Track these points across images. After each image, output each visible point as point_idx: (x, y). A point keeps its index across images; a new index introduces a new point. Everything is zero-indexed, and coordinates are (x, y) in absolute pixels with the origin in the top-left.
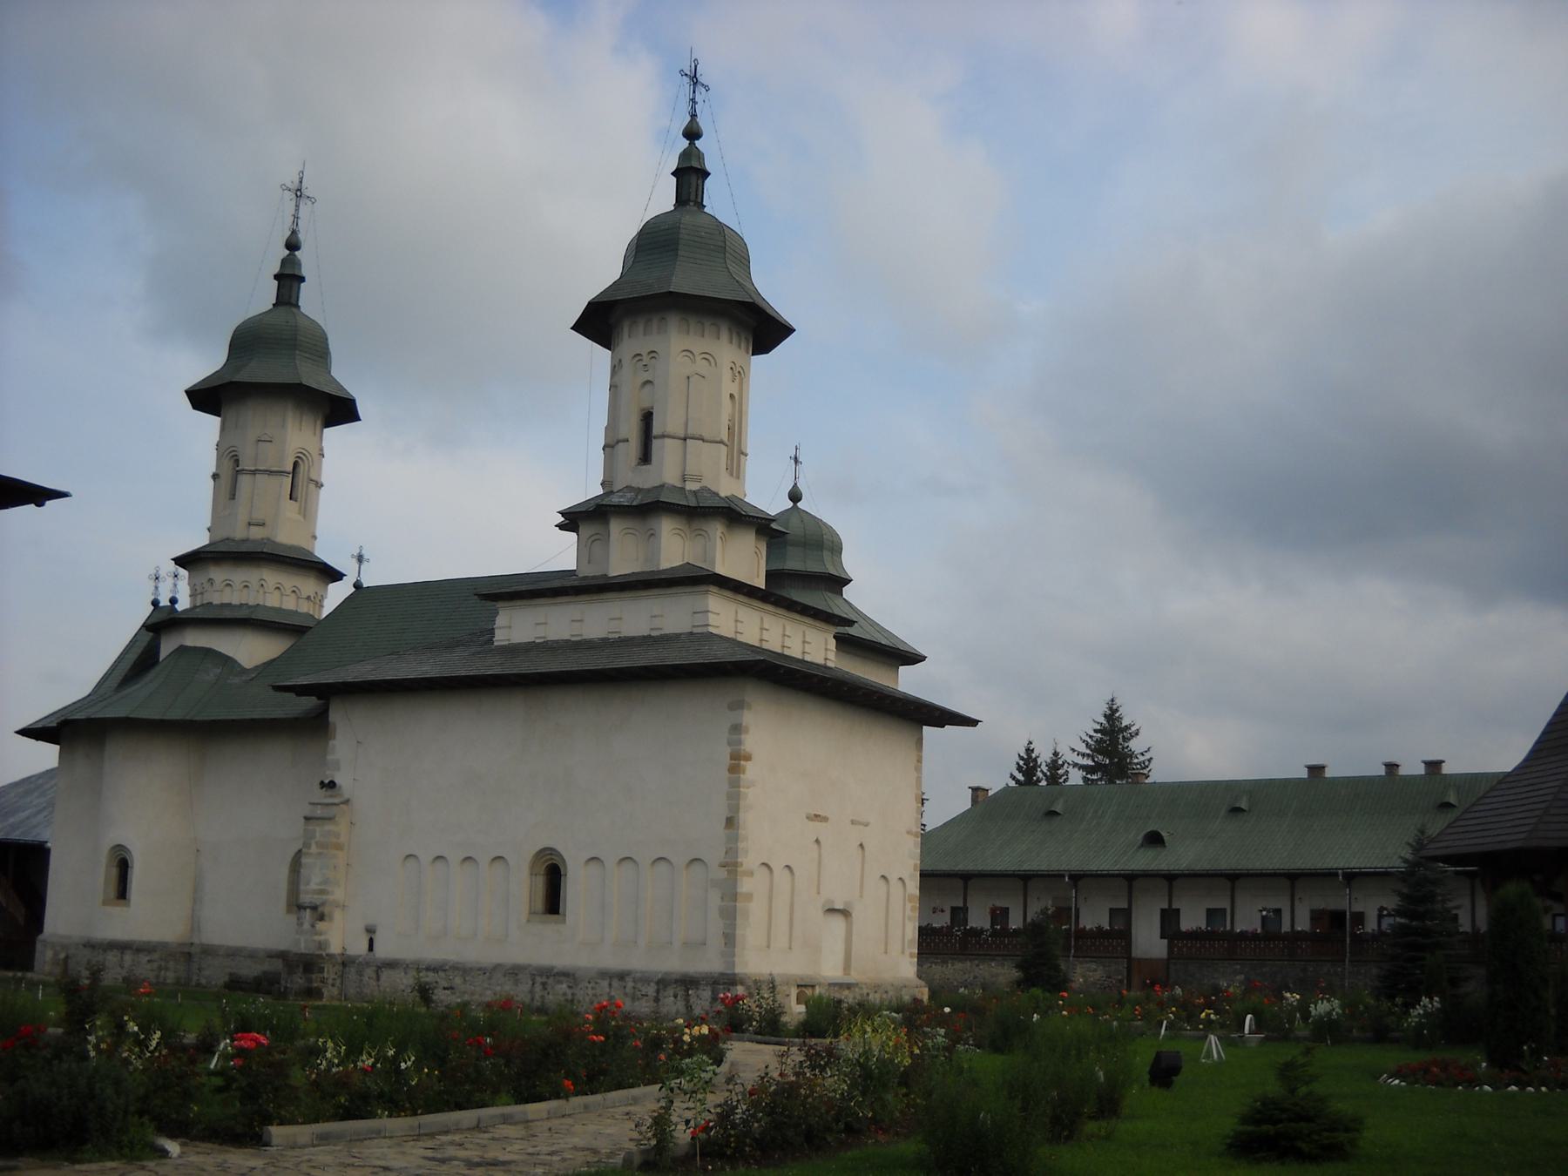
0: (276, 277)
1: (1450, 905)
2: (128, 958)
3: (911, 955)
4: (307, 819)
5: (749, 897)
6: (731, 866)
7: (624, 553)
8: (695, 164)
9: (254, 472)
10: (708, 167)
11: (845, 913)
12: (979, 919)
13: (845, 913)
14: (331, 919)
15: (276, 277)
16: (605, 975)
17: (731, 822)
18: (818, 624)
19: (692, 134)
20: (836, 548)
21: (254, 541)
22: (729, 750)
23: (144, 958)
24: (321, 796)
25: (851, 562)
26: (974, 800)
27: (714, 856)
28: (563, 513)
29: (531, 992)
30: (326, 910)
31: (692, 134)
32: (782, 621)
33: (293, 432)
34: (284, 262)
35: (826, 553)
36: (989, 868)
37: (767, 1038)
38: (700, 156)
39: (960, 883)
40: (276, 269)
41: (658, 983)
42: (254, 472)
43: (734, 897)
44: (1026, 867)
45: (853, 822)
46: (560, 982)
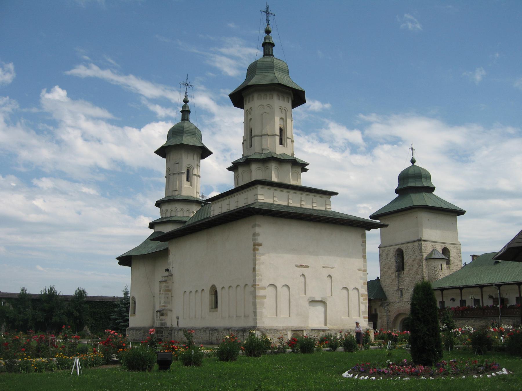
2: (135, 332)
3: (364, 318)
4: (160, 282)
5: (264, 297)
6: (254, 286)
11: (323, 302)
12: (470, 303)
13: (323, 302)
14: (167, 315)
15: (181, 112)
16: (205, 329)
17: (254, 269)
18: (239, 193)
19: (268, 32)
20: (428, 177)
22: (252, 243)
23: (138, 332)
24: (167, 273)
25: (434, 181)
26: (473, 259)
27: (250, 284)
29: (209, 337)
30: (164, 312)
31: (268, 32)
32: (300, 196)
33: (187, 160)
35: (423, 179)
36: (471, 284)
39: (479, 290)
41: (237, 331)
43: (255, 297)
44: (480, 283)
45: (323, 267)
46: (215, 333)
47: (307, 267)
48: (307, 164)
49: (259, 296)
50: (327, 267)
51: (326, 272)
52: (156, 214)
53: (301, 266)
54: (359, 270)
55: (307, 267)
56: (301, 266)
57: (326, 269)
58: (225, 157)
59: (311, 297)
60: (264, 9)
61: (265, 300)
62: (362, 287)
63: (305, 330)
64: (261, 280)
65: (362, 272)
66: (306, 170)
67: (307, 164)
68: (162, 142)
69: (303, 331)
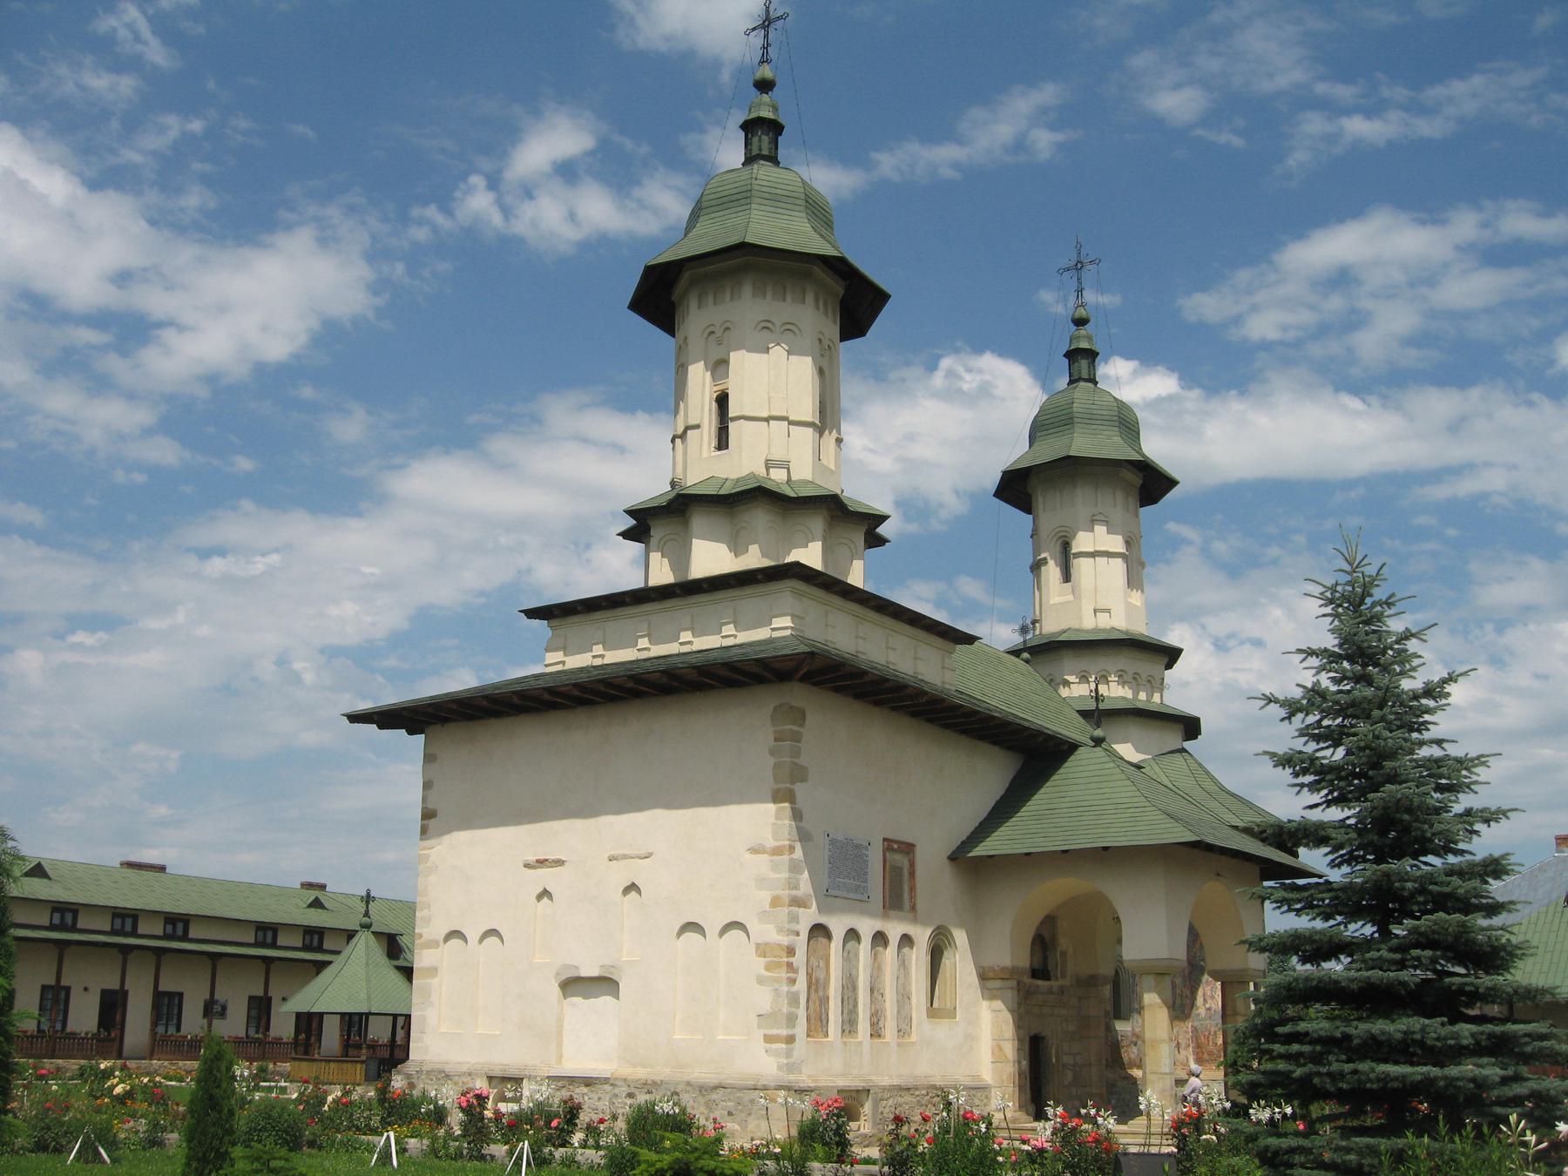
5: (433, 971)
9: (1093, 555)
21: (1104, 630)
28: (631, 513)
42: (1093, 555)
47: (560, 863)
49: (422, 969)
50: (625, 857)
51: (622, 874)
52: (771, 761)
53: (541, 863)
54: (755, 850)
55: (560, 863)
56: (541, 863)
58: (1203, 627)
61: (435, 981)
62: (763, 916)
63: (529, 1078)
64: (428, 920)
65: (765, 857)
68: (1014, 451)
69: (518, 1081)
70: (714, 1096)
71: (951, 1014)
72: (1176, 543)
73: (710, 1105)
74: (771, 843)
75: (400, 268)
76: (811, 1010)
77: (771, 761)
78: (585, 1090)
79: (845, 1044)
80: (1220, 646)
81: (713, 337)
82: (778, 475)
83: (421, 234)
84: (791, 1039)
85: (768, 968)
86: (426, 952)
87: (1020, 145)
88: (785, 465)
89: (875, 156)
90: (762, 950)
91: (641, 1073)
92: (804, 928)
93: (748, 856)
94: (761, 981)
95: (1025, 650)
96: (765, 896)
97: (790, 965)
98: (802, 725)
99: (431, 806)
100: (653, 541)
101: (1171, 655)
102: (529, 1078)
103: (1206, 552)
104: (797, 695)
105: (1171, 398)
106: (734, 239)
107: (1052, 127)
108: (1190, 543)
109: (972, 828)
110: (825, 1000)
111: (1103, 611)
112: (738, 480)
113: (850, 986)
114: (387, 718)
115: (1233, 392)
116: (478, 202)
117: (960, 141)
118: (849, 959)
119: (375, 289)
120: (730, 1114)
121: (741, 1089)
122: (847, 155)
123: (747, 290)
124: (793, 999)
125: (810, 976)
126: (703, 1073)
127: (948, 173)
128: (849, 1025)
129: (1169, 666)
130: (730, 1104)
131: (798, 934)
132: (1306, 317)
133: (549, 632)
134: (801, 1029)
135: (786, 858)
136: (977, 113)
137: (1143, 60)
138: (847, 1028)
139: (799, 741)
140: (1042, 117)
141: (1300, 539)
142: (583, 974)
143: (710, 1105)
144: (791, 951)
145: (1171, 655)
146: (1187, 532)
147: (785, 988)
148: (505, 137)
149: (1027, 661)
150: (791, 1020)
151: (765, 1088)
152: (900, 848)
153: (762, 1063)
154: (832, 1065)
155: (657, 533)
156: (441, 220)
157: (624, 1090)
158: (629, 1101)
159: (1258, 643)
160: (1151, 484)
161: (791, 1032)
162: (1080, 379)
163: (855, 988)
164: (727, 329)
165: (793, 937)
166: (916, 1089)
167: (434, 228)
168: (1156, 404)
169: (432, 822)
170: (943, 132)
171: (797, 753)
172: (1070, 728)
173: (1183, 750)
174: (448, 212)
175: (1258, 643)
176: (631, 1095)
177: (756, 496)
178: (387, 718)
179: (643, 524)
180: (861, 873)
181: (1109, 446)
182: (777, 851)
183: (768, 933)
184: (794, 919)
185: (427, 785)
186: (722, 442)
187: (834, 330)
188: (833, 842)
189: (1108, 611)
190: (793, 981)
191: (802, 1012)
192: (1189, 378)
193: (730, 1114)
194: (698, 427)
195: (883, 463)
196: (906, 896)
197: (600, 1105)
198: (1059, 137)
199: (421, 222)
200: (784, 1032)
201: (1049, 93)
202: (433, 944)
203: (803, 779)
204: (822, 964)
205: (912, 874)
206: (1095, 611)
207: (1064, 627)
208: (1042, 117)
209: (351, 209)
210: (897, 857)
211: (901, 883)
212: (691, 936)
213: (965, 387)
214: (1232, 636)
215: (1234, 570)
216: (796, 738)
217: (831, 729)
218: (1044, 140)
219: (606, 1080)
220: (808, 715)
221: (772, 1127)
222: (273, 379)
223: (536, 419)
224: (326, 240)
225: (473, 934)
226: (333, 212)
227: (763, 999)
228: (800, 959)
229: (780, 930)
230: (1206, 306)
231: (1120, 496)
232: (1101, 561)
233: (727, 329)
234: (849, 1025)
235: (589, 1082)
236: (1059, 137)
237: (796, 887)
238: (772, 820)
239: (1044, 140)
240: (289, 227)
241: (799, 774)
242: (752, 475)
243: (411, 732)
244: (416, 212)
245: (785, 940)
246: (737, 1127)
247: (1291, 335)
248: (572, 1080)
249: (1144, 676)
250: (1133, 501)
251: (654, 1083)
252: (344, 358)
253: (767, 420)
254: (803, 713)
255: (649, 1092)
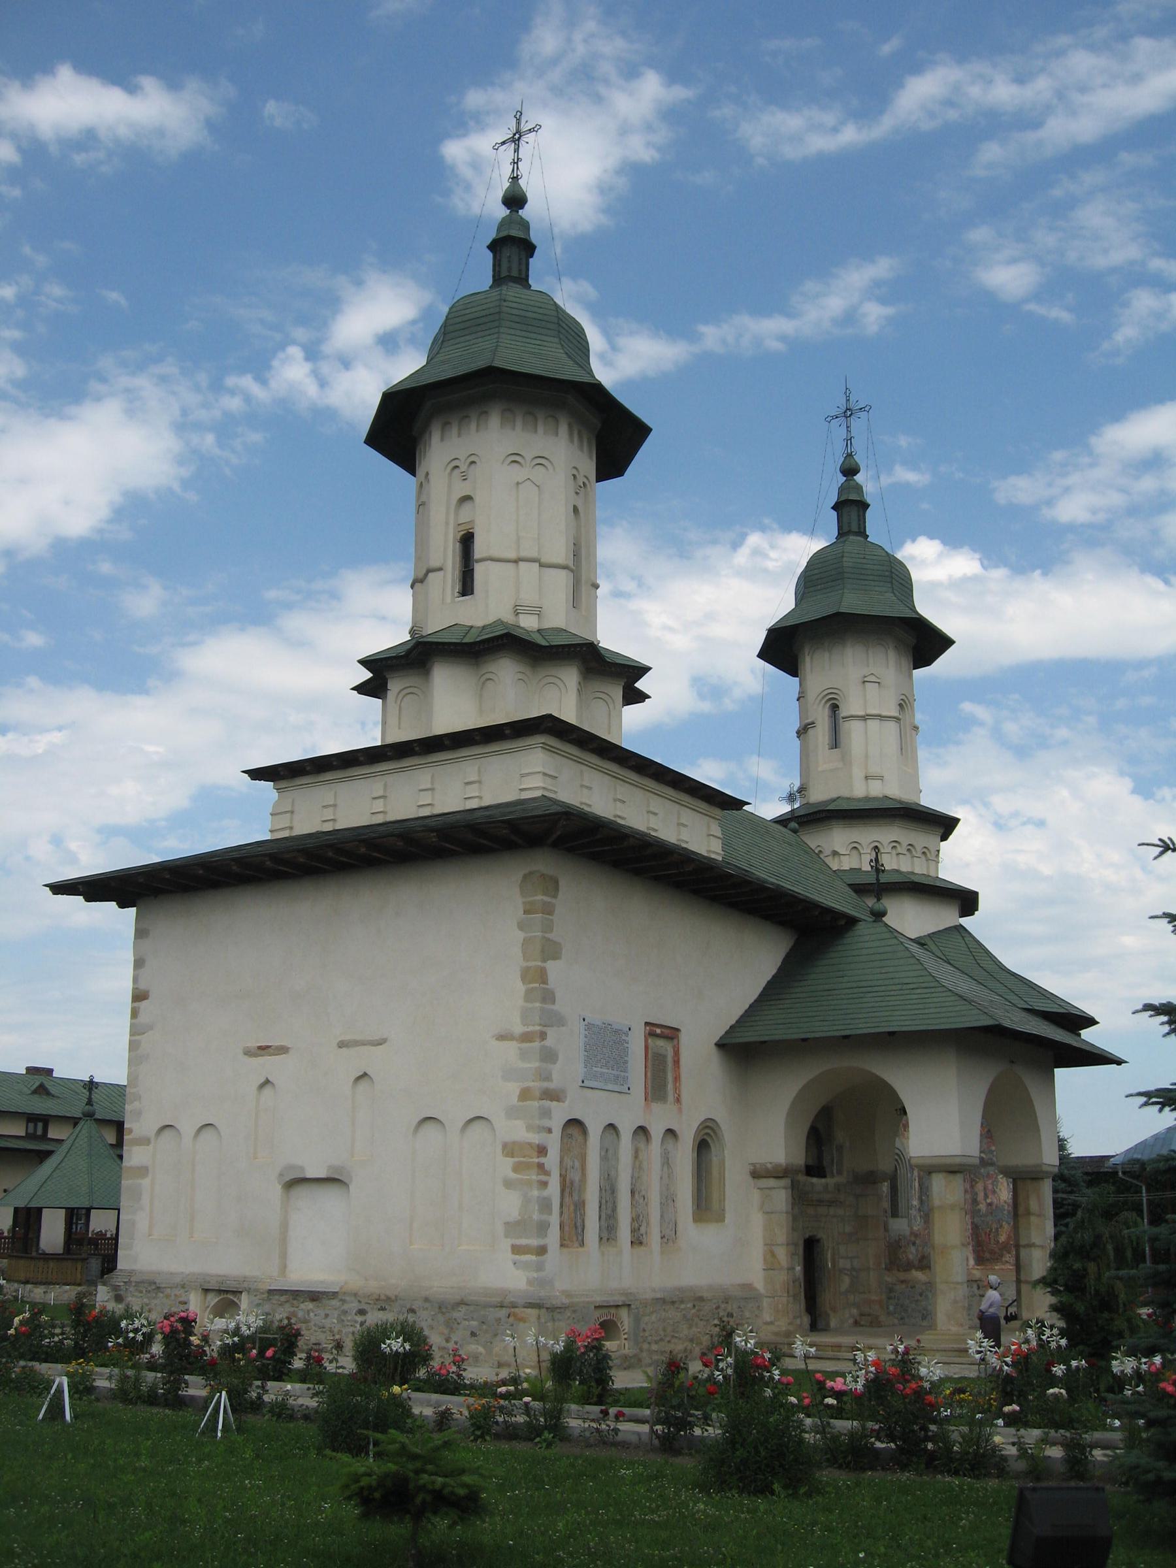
0: (835, 507)
1: (1088, 1437)
5: (143, 1171)
7: (452, 701)
8: (853, 497)
9: (864, 718)
10: (869, 501)
19: (850, 471)
21: (875, 799)
28: (366, 663)
31: (850, 471)
34: (842, 490)
37: (649, 1082)
38: (859, 488)
40: (834, 499)
42: (864, 718)
45: (342, 1045)
47: (283, 1050)
48: (643, 670)
49: (131, 1168)
52: (521, 935)
53: (264, 1049)
54: (501, 1037)
55: (283, 1050)
56: (264, 1049)
57: (353, 1051)
59: (291, 1167)
60: (859, 398)
61: (145, 1182)
62: (512, 1113)
63: (249, 1291)
64: (138, 1113)
65: (514, 1045)
66: (641, 697)
67: (643, 670)
70: (456, 1314)
71: (720, 1218)
72: (969, 722)
73: (451, 1325)
74: (518, 1029)
75: (210, 438)
76: (566, 1216)
77: (521, 935)
78: (310, 1305)
79: (603, 1254)
80: (999, 825)
81: (456, 471)
82: (528, 623)
83: (234, 404)
84: (542, 1250)
85: (517, 1168)
86: (136, 1149)
87: (850, 318)
88: (538, 612)
89: (704, 329)
90: (510, 1149)
91: (373, 1287)
92: (557, 1123)
93: (494, 1043)
94: (508, 1184)
95: (790, 820)
96: (513, 1089)
97: (541, 1166)
98: (555, 896)
99: (142, 986)
100: (391, 695)
101: (946, 825)
102: (249, 1291)
103: (997, 734)
104: (543, 863)
105: (975, 579)
106: (481, 363)
107: (883, 301)
108: (982, 724)
109: (740, 1012)
110: (580, 1206)
111: (874, 778)
112: (484, 627)
113: (609, 1190)
114: (94, 888)
115: (1038, 572)
116: (293, 371)
117: (790, 315)
118: (608, 1156)
119: (180, 461)
120: (473, 1334)
121: (487, 1306)
122: (669, 322)
123: (494, 420)
124: (545, 1205)
125: (563, 1177)
126: (442, 1284)
127: (775, 345)
128: (608, 1233)
129: (944, 838)
130: (474, 1323)
131: (550, 1131)
132: (1116, 499)
133: (275, 795)
134: (553, 1238)
135: (536, 1044)
136: (810, 286)
137: (979, 235)
138: (605, 1235)
139: (551, 913)
140: (881, 291)
141: (1092, 720)
142: (309, 1175)
143: (451, 1325)
144: (542, 1150)
145: (946, 825)
146: (980, 711)
147: (536, 1193)
148: (329, 305)
149: (795, 831)
150: (543, 1228)
151: (514, 1306)
152: (663, 1033)
153: (506, 1275)
154: (591, 1274)
155: (395, 686)
156: (256, 390)
157: (354, 1306)
158: (360, 1319)
159: (1041, 824)
160: (926, 643)
161: (541, 1242)
162: (849, 532)
163: (613, 1191)
164: (473, 462)
165: (544, 1135)
166: (682, 1302)
167: (248, 399)
168: (958, 584)
169: (143, 1005)
170: (772, 302)
171: (548, 927)
172: (840, 900)
173: (960, 928)
174: (262, 381)
175: (1041, 824)
176: (362, 1312)
177: (505, 643)
178: (94, 888)
179: (381, 674)
180: (620, 1062)
181: (880, 604)
182: (526, 1038)
183: (519, 1131)
184: (546, 1113)
185: (139, 964)
186: (467, 586)
187: (589, 466)
188: (589, 1027)
189: (881, 778)
190: (544, 1184)
191: (554, 1219)
192: (991, 556)
193: (473, 1334)
194: (440, 569)
195: (680, 642)
196: (670, 1086)
197: (327, 1323)
198: (889, 311)
199: (232, 392)
200: (534, 1242)
201: (882, 268)
202: (145, 1141)
203: (556, 956)
204: (577, 1164)
205: (677, 1062)
206: (866, 778)
207: (834, 795)
208: (881, 291)
209: (163, 379)
210: (661, 1043)
211: (664, 1071)
212: (430, 1129)
213: (770, 565)
214: (1015, 814)
215: (1022, 752)
216: (548, 910)
217: (590, 907)
218: (874, 314)
219: (335, 1294)
220: (562, 883)
221: (526, 1349)
222: (70, 555)
223: (334, 595)
224: (134, 408)
225: (187, 1128)
226: (142, 382)
227: (511, 1205)
228: (552, 1160)
229: (529, 1128)
230: (1020, 489)
231: (892, 654)
232: (873, 724)
233: (473, 462)
234: (608, 1233)
235: (315, 1297)
236: (889, 311)
237: (548, 1078)
238: (521, 1002)
239: (874, 314)
240: (98, 399)
241: (551, 951)
242: (499, 622)
243: (122, 905)
244: (231, 381)
245: (535, 1138)
246: (481, 1349)
247: (1101, 517)
248: (296, 1295)
249: (919, 848)
250: (906, 662)
251: (388, 1299)
252: (148, 533)
253: (516, 561)
254: (557, 882)
255: (383, 1309)
